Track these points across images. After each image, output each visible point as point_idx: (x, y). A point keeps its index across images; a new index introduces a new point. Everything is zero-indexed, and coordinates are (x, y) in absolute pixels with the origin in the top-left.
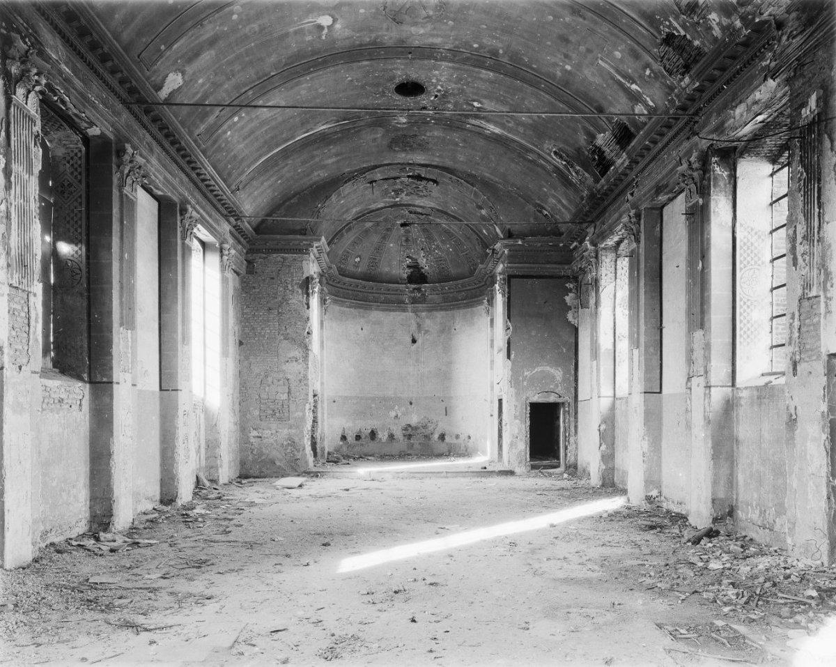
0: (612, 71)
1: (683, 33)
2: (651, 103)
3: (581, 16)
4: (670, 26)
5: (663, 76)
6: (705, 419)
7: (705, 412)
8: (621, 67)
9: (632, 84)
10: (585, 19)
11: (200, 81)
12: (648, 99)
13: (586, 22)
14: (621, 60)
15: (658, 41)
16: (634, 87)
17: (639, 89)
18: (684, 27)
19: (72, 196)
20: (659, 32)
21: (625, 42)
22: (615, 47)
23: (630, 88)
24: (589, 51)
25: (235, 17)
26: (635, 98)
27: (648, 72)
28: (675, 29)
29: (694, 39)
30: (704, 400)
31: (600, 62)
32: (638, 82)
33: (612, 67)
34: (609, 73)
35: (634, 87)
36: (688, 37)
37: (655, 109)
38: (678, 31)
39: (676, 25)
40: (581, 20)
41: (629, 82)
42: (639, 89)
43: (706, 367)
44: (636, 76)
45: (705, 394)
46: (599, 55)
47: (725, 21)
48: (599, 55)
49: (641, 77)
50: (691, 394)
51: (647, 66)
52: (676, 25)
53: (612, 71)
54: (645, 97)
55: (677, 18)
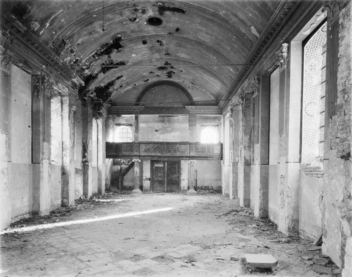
0: (56, 15)
1: (66, 48)
2: (41, 33)
3: (83, 13)
4: (68, 44)
5: (52, 39)
6: (49, 175)
7: (49, 172)
8: (57, 20)
9: (50, 24)
10: (81, 13)
11: (250, 15)
12: (43, 31)
13: (80, 13)
14: (60, 21)
15: (64, 38)
16: (48, 24)
17: (47, 27)
18: (68, 49)
19: (309, 70)
20: (66, 40)
21: (67, 25)
22: (66, 20)
23: (47, 22)
24: (69, 8)
25: (224, 12)
26: (42, 23)
27: (54, 33)
28: (67, 46)
29: (64, 52)
30: (49, 168)
31: (62, 10)
32: (50, 27)
33: (58, 16)
34: (55, 13)
35: (48, 24)
36: (64, 50)
37: (38, 35)
38: (66, 47)
39: (68, 46)
40: (82, 12)
41: (50, 22)
42: (47, 27)
43: (49, 157)
44: (53, 26)
45: (49, 166)
46: (65, 12)
47: (68, 62)
48: (65, 12)
49: (52, 29)
50: (43, 165)
51: (56, 33)
52: (68, 46)
53: (56, 15)
54: (44, 29)
55: (70, 47)
